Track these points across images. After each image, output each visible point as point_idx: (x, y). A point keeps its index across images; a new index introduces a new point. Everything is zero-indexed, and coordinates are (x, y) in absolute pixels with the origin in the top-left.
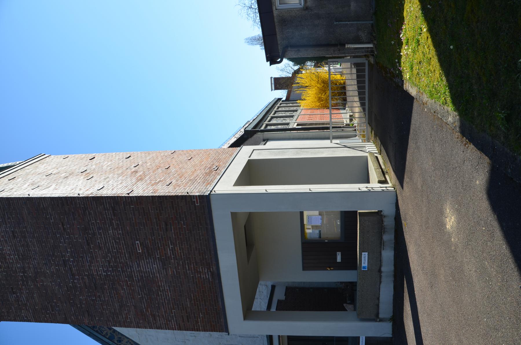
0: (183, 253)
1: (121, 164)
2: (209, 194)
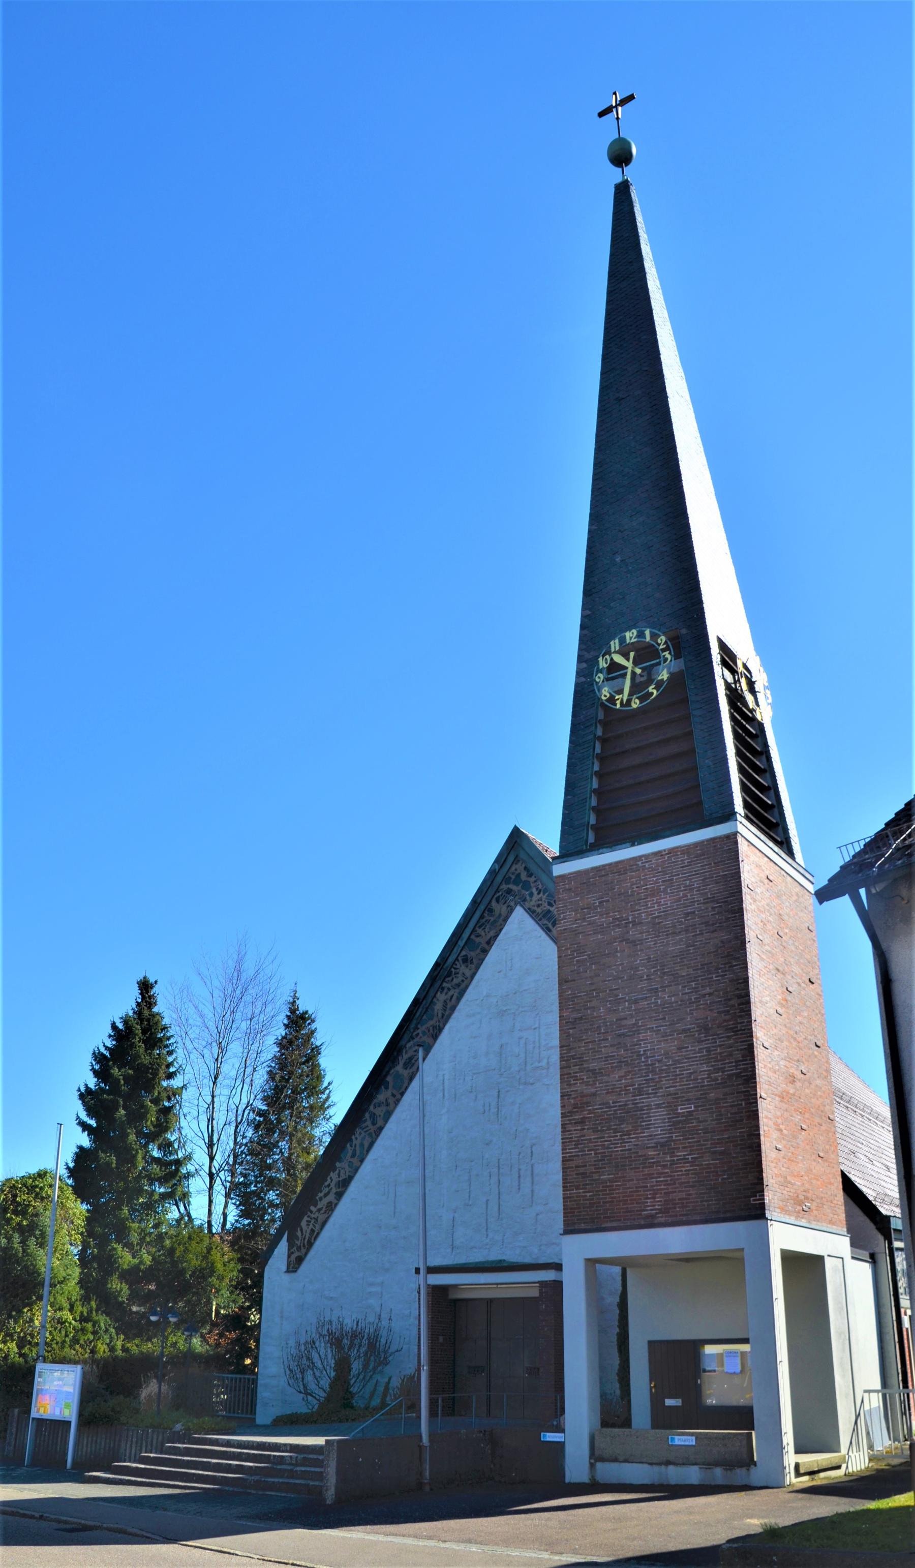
2: (767, 1219)
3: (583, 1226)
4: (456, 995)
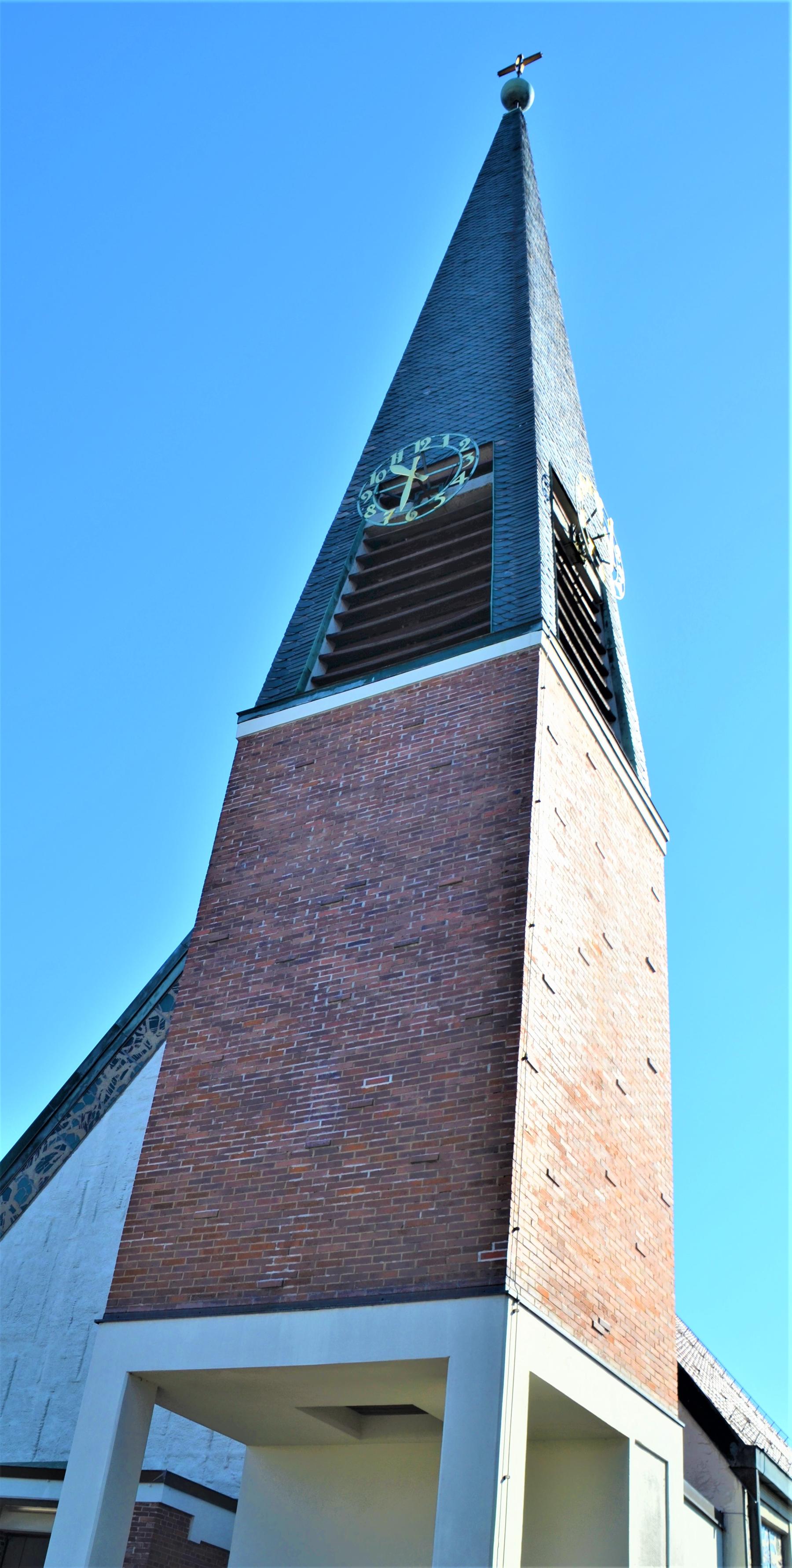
0: (346, 1207)
1: (630, 1045)
2: (507, 1294)
3: (141, 1307)
4: (131, 1070)
